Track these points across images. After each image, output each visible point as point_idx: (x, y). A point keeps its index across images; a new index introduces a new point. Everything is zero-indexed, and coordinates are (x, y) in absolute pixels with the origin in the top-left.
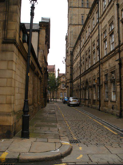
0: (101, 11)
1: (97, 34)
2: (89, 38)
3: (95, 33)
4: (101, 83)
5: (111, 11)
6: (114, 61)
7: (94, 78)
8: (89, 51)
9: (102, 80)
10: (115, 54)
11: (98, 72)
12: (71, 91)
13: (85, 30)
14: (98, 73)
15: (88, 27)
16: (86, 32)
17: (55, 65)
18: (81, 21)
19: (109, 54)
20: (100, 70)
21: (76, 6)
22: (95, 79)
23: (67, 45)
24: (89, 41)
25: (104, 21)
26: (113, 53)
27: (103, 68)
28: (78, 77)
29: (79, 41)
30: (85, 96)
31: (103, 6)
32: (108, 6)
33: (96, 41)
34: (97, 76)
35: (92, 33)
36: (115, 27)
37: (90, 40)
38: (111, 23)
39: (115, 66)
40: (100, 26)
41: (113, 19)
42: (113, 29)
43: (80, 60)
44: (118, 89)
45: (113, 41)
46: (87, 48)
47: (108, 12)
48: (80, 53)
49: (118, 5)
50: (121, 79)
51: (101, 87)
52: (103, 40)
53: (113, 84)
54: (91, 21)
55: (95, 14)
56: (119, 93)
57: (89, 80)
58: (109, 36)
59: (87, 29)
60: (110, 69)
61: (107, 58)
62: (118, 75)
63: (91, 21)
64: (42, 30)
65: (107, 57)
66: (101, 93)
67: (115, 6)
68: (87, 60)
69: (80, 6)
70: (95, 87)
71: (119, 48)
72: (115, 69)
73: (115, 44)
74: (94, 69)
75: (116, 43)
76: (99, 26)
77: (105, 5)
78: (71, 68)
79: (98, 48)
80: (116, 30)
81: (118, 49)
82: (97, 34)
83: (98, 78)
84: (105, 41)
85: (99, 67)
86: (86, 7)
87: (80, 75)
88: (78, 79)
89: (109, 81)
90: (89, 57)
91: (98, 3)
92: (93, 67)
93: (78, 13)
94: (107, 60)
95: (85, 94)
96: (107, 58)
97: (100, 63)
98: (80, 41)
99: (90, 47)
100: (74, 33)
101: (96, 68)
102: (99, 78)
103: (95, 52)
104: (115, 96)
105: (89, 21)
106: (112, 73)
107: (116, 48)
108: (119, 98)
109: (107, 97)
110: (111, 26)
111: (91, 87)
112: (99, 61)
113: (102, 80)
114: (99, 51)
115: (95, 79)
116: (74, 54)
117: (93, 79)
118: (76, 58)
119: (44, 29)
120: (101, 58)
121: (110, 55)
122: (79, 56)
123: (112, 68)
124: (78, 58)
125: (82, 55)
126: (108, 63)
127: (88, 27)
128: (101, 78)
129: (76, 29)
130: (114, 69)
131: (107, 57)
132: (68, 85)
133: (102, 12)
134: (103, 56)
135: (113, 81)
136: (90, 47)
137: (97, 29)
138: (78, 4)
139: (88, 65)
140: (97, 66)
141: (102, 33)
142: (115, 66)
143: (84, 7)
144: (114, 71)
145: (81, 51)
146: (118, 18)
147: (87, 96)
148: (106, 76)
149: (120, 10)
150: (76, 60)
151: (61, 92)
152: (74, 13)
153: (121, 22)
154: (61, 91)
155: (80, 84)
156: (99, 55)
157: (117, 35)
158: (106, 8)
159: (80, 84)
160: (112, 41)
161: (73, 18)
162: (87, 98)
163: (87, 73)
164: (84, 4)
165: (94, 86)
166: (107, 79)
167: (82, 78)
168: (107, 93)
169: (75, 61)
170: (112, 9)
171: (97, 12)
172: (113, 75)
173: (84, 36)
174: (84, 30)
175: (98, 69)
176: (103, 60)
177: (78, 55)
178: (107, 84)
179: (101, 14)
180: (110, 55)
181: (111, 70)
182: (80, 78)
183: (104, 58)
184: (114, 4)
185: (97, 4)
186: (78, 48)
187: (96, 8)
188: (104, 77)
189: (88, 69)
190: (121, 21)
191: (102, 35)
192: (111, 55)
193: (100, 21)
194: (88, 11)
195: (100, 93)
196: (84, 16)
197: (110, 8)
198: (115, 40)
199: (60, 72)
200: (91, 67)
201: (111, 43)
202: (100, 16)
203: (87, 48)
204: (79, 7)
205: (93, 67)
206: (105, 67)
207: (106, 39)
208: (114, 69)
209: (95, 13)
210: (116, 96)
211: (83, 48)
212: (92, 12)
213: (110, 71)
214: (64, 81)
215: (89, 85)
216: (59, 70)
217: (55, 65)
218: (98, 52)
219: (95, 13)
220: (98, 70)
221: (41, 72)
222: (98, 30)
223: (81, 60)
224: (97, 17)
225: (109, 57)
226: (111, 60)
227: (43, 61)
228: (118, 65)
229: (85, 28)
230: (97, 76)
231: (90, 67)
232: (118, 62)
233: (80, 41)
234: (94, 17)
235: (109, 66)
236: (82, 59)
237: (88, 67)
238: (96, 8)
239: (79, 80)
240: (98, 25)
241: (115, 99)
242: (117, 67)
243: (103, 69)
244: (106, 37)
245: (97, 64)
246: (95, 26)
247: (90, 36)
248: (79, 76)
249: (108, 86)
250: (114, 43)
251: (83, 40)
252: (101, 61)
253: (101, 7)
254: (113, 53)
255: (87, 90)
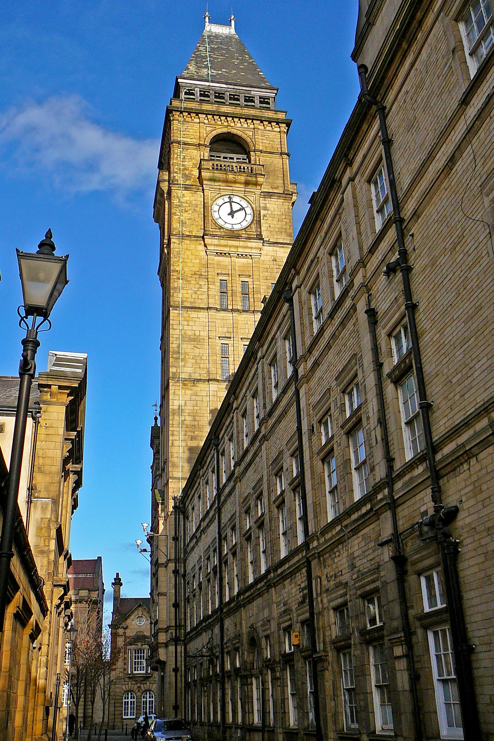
0: (303, 333)
1: (289, 425)
2: (257, 444)
3: (283, 423)
4: (320, 646)
5: (346, 333)
6: (372, 544)
7: (287, 624)
8: (259, 497)
9: (324, 635)
10: (375, 515)
11: (304, 597)
12: (179, 685)
13: (237, 408)
14: (302, 602)
15: (249, 396)
16: (244, 416)
17: (100, 558)
18: (219, 366)
19: (348, 513)
20: (310, 586)
21: (197, 305)
22: (290, 626)
23: (157, 469)
24: (255, 455)
25: (318, 373)
26: (364, 510)
27: (324, 578)
28: (209, 617)
29: (213, 452)
30: (247, 711)
31: (310, 314)
32: (331, 316)
33: (287, 454)
34: (298, 615)
35: (272, 421)
36: (366, 400)
37: (234, 488)
38: (349, 384)
39: (378, 568)
40: (302, 392)
41: (357, 366)
42: (359, 408)
43: (217, 536)
44: (398, 675)
45: (362, 457)
46: (245, 487)
47: (334, 337)
48: (219, 503)
49: (371, 313)
50: (409, 629)
51: (319, 667)
52: (318, 454)
53: (374, 652)
54: (263, 371)
55: (279, 343)
56: (408, 695)
57: (262, 634)
58: (344, 437)
59: (248, 403)
60: (356, 581)
61: (338, 533)
62: (397, 610)
63: (263, 371)
64: (51, 408)
65: (338, 528)
66: (321, 696)
67: (362, 316)
68: (249, 539)
69: (215, 302)
70: (292, 667)
71: (391, 491)
72: (378, 584)
73: (372, 469)
74: (283, 578)
75: (377, 468)
76: (297, 392)
77: (321, 311)
78: (176, 572)
79: (297, 487)
80: (371, 414)
81: (386, 491)
82: (289, 425)
83: (303, 623)
84: (327, 455)
85: (304, 570)
86: (239, 308)
87: (221, 608)
88: (210, 627)
89: (356, 638)
90: (261, 525)
91: (290, 300)
92: (279, 571)
93: (204, 334)
94: (340, 542)
95: (247, 700)
96: (341, 530)
97: (307, 558)
98: (218, 452)
99: (261, 479)
100: (191, 418)
101: (292, 574)
102: (310, 624)
103: (283, 502)
104: (389, 710)
105: (253, 371)
106: (368, 597)
107: (377, 489)
108: (407, 719)
109: (352, 712)
110: (350, 394)
111: (269, 664)
112: (306, 544)
113: (324, 635)
114: (304, 498)
115: (290, 626)
116: (190, 508)
117: (282, 626)
118: (197, 530)
119: (62, 404)
120: (311, 529)
121: (355, 516)
122: (211, 521)
123: (364, 579)
124: (208, 526)
125: (225, 517)
126: (345, 554)
127: (249, 396)
128: (319, 623)
129: (198, 398)
130: (373, 581)
131: (338, 528)
132: (162, 654)
133: (307, 335)
134: (323, 524)
135: (373, 638)
136: (261, 479)
137: (288, 406)
138: (205, 297)
139: (256, 562)
140: (298, 569)
141: (315, 422)
142: (378, 568)
143: (230, 307)
144: (376, 590)
145: (222, 498)
146: (379, 366)
147: (256, 712)
148: (342, 613)
149: (382, 332)
150: (198, 535)
151: (127, 692)
152: (189, 333)
153: (389, 381)
154: (130, 685)
155: (222, 649)
156: (304, 519)
157: (379, 432)
158: (325, 323)
159: (222, 649)
160: (357, 459)
161: (186, 354)
162: (256, 719)
163: (251, 600)
164: (229, 294)
165: (288, 660)
166: (343, 626)
167: (228, 623)
168: (350, 695)
169: (197, 543)
170: (350, 325)
171: (288, 331)
172: (374, 609)
173: (235, 432)
174: (235, 406)
175: (301, 578)
176: (322, 540)
177: (208, 512)
178: (350, 654)
179: (303, 344)
180: (355, 516)
181: (363, 586)
182: (222, 622)
183: (324, 532)
184: (355, 310)
185: (286, 305)
186: (207, 483)
187: (285, 316)
188: (332, 617)
189: (257, 581)
190: (389, 375)
191: (312, 430)
192: (355, 519)
193: (301, 372)
194: (249, 324)
195: (315, 694)
196: (230, 342)
197: (343, 324)
198: (370, 455)
199: (126, 592)
200: (268, 572)
201: (353, 466)
202: (300, 352)
203: (245, 487)
204: (208, 308)
205: (279, 571)
206: (332, 573)
207: (332, 450)
208: (373, 581)
209: (280, 336)
210: (396, 713)
211: (232, 483)
212: (265, 334)
213: (359, 592)
214: (145, 637)
215: (265, 656)
216: (118, 582)
217: (100, 558)
218: (297, 503)
219: (280, 336)
220: (303, 585)
221: (40, 599)
222: (293, 410)
223: (222, 538)
224: (288, 355)
225: (346, 526)
226: (356, 542)
227: (49, 551)
228: (391, 566)
229: (236, 398)
230: (298, 615)
231: (263, 572)
232: (387, 553)
233: (218, 452)
234: (275, 355)
235: (353, 566)
236: (229, 535)
237: (254, 572)
238: (285, 316)
239: (217, 630)
240: (293, 388)
241: (391, 726)
242: (389, 573)
243: (325, 582)
244: (329, 441)
245: (296, 559)
246: (280, 391)
247: (259, 431)
248: (214, 612)
249: (350, 661)
250: (368, 467)
251: (227, 464)
252: (315, 543)
253: (301, 318)
254: (364, 510)
255: (253, 679)
